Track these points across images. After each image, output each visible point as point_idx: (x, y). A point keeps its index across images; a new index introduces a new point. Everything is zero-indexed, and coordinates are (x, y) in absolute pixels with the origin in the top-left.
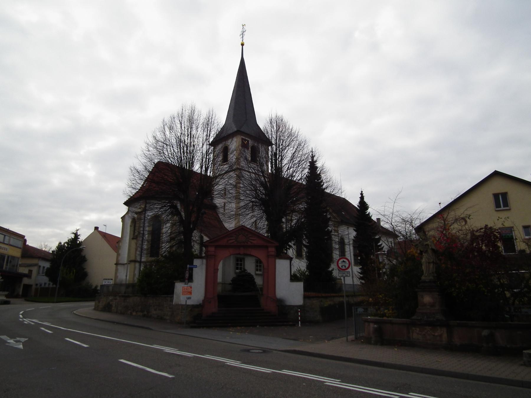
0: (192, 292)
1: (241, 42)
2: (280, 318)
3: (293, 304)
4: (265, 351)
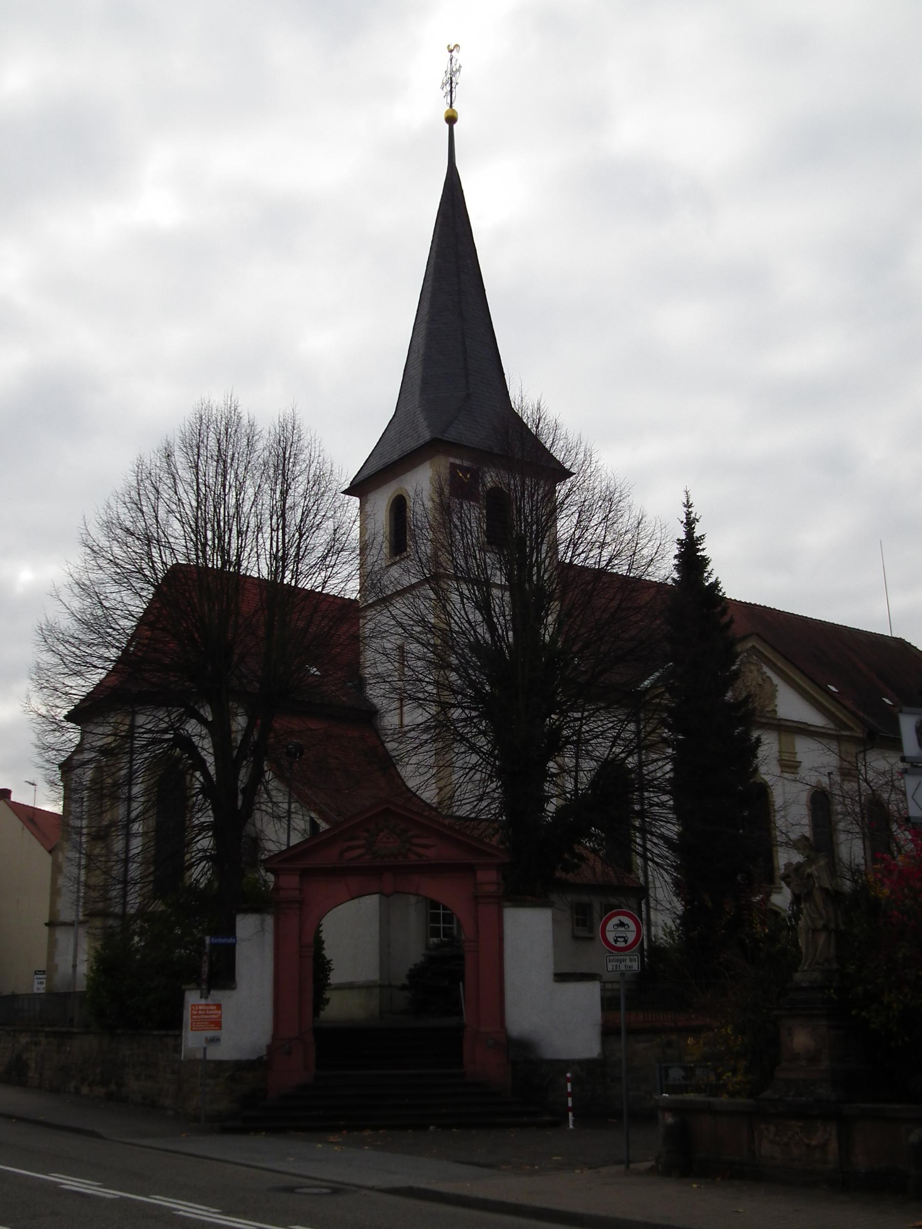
0: (236, 1020)
1: (443, 109)
2: (524, 1098)
3: (564, 1056)
4: (337, 1190)
